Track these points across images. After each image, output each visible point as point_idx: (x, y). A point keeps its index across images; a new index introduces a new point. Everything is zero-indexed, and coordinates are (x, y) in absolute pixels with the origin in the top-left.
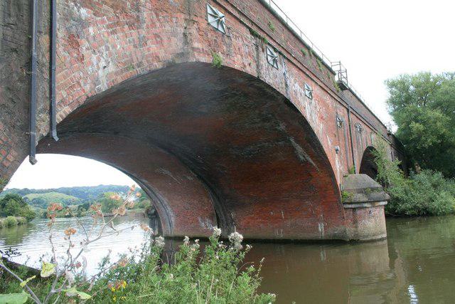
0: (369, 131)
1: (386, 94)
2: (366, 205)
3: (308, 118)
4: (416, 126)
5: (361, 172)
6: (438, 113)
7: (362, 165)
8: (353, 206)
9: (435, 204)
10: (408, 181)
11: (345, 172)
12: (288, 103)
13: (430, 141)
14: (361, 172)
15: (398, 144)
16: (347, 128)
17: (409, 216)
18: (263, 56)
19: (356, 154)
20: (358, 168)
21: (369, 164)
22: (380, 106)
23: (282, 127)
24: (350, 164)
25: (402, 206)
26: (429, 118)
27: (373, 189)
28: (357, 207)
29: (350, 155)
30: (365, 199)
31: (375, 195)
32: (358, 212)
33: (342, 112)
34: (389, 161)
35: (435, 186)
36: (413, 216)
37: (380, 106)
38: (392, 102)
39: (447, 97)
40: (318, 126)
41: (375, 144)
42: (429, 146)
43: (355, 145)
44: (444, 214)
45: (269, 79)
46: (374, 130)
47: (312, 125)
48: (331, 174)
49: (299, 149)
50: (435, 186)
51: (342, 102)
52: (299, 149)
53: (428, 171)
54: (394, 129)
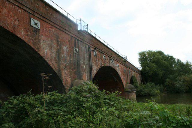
0: (132, 71)
1: (138, 57)
2: (131, 92)
3: (118, 72)
4: (147, 68)
5: (130, 84)
6: (153, 65)
7: (130, 81)
8: (73, 35)
9: (151, 92)
10: (144, 85)
11: (126, 84)
12: (114, 69)
13: (151, 73)
14: (130, 84)
15: (142, 73)
16: (126, 72)
17: (143, 96)
18: (110, 61)
19: (129, 79)
20: (129, 83)
21: (132, 81)
22: (138, 65)
23: (112, 73)
24: (127, 81)
25: (142, 93)
26: (151, 66)
27: (133, 88)
28: (129, 92)
29: (127, 79)
30: (131, 90)
31: (133, 89)
32: (129, 94)
33: (125, 68)
34: (138, 77)
35: (152, 87)
36: (145, 96)
37: (138, 65)
38: (140, 59)
39: (157, 59)
40: (120, 73)
41: (135, 76)
42: (151, 75)
43: (128, 76)
44: (154, 95)
45: (111, 66)
46: (134, 71)
47: (119, 73)
48: (123, 85)
49: (115, 78)
50: (152, 87)
51: (125, 65)
52: (115, 78)
53: (151, 82)
54: (141, 69)
